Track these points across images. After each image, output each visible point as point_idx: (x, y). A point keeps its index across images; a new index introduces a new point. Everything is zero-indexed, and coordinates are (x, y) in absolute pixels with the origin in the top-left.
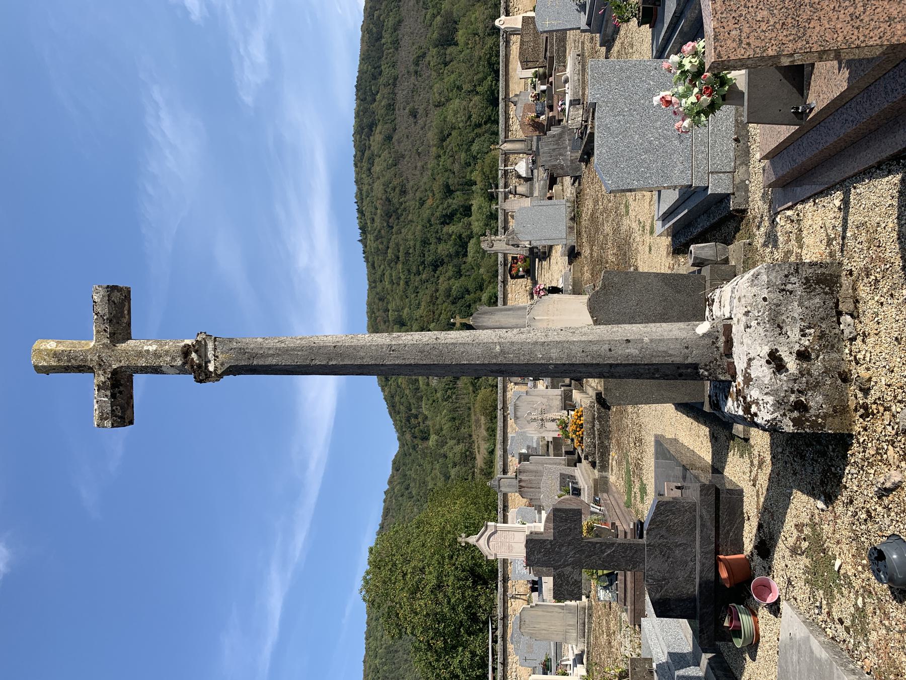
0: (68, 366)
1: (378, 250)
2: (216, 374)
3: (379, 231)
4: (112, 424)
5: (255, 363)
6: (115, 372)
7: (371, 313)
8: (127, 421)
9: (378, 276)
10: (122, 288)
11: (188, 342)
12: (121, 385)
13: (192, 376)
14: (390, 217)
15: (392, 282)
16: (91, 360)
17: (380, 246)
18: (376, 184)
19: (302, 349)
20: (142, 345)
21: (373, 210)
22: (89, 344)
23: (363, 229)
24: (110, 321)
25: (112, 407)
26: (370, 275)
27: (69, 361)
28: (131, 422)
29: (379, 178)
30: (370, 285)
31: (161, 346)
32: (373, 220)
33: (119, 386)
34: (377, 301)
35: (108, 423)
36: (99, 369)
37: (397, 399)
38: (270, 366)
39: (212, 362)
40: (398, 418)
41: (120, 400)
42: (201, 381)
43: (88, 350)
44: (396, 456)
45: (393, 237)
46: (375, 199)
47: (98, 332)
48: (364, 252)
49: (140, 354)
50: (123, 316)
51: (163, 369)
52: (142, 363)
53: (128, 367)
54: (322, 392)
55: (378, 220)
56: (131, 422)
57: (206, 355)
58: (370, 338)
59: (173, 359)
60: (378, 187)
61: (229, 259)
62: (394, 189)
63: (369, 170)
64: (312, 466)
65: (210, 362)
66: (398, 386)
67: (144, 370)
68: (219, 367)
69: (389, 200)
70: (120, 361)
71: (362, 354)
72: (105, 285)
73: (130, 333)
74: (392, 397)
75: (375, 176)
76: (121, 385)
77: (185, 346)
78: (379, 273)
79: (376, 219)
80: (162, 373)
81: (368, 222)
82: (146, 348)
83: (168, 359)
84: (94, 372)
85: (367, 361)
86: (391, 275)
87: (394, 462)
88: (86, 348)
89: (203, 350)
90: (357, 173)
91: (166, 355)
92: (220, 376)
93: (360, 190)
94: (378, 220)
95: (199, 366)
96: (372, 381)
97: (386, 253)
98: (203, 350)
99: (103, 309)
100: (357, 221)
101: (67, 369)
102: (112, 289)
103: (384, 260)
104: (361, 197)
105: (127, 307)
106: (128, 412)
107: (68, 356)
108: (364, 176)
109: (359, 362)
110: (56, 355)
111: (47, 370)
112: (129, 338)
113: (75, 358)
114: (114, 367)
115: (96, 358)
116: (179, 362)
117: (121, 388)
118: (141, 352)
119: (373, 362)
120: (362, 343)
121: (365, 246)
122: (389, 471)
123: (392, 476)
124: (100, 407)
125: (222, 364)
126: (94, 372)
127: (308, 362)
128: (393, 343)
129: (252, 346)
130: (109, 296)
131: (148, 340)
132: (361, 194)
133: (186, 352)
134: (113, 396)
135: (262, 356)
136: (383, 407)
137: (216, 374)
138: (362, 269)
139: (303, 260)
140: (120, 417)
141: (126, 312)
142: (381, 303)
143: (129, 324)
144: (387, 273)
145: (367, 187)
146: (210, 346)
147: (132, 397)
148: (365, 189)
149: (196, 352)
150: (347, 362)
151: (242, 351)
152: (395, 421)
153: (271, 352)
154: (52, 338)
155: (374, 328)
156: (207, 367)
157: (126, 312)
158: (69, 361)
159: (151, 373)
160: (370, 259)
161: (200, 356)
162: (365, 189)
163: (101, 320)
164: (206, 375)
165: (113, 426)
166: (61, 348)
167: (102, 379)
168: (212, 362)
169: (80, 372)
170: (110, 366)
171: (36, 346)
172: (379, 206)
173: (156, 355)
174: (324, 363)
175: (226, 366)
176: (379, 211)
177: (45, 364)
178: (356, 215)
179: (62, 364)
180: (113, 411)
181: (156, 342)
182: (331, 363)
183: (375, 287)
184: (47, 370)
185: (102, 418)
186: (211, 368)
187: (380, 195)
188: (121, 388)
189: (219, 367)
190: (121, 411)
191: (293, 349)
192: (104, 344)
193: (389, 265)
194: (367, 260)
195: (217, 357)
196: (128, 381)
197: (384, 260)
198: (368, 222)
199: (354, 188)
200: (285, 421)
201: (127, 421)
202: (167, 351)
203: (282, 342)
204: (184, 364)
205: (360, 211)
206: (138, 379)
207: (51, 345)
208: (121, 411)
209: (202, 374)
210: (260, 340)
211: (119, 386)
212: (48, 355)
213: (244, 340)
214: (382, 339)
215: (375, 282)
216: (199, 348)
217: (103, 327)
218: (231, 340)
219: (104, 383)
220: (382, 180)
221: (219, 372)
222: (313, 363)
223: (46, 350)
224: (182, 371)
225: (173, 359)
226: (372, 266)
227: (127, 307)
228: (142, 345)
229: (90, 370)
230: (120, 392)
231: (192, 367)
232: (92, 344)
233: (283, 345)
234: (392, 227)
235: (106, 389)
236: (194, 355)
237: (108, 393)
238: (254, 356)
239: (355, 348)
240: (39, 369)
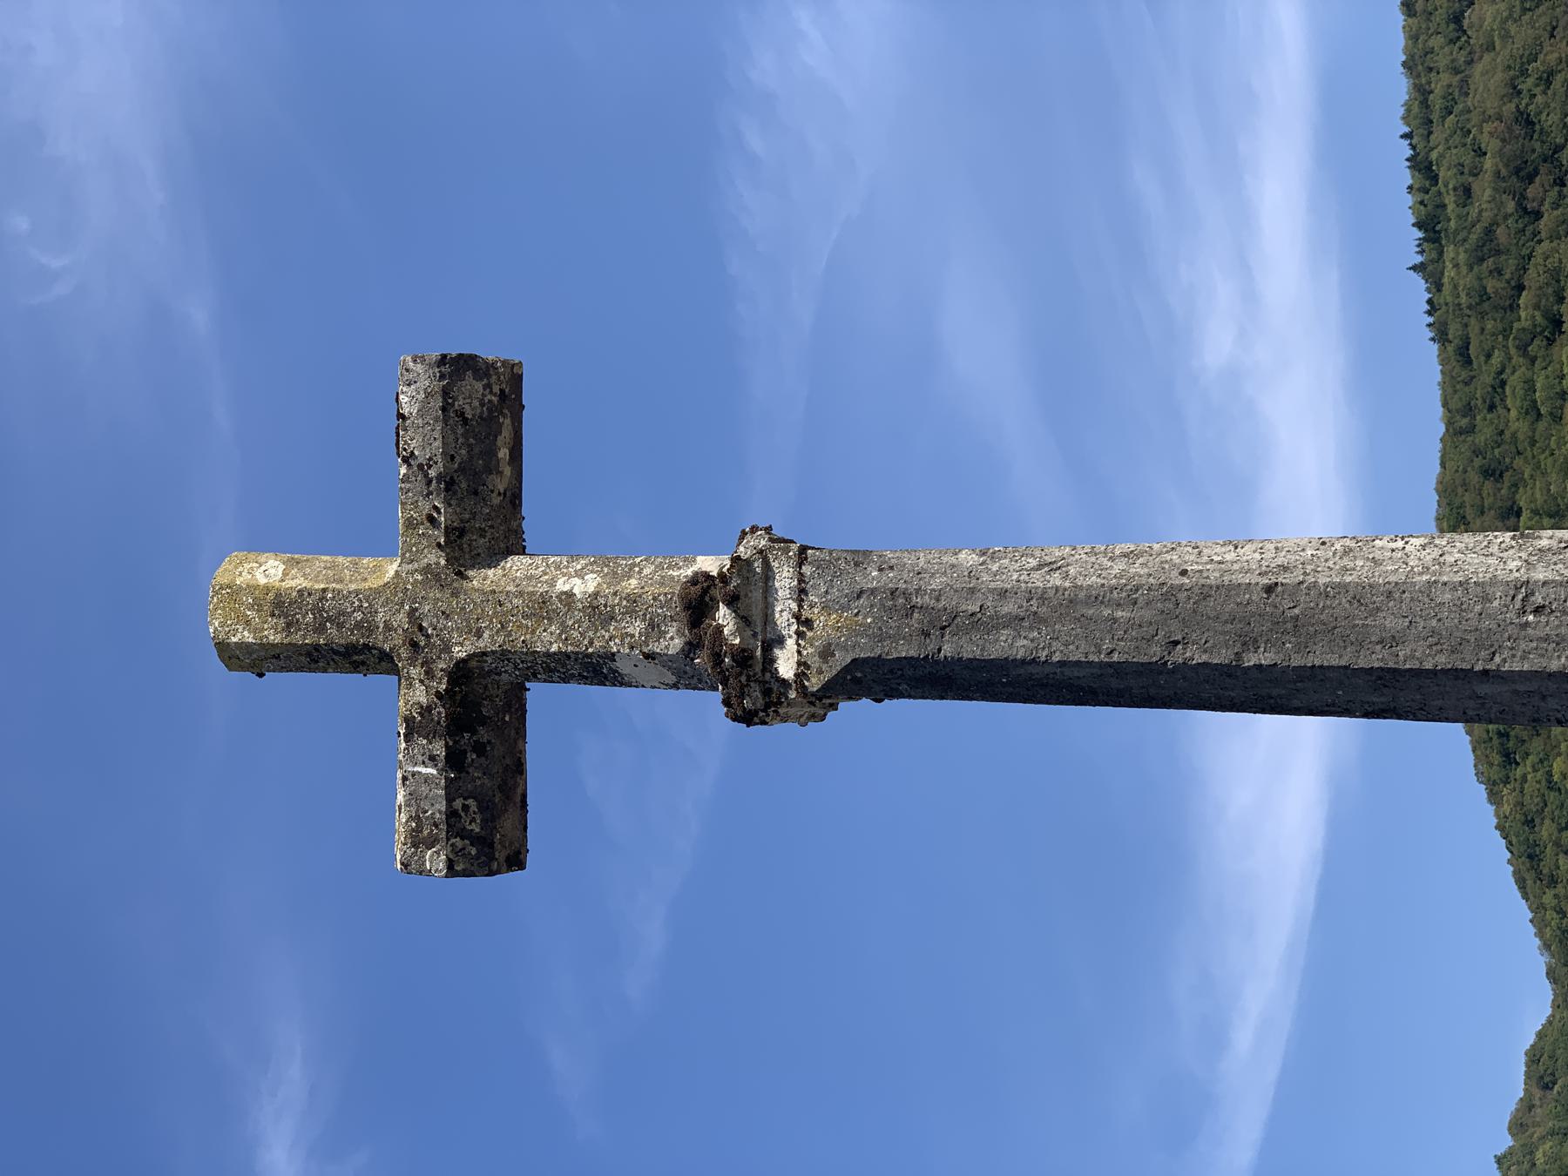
0: (317, 647)
1: (1484, 296)
2: (802, 690)
3: (1489, 231)
4: (450, 865)
5: (948, 650)
6: (461, 673)
7: (1447, 490)
8: (501, 855)
9: (1480, 390)
10: (491, 366)
11: (710, 564)
12: (483, 721)
13: (718, 696)
14: (1530, 178)
15: (1532, 411)
16: (388, 627)
17: (1491, 285)
18: (1478, 68)
19: (1130, 594)
20: (552, 579)
21: (1468, 159)
22: (377, 573)
23: (1430, 227)
24: (449, 484)
25: (450, 799)
26: (1450, 386)
27: (320, 629)
28: (516, 861)
29: (1490, 47)
30: (1449, 423)
31: (615, 577)
32: (1467, 191)
33: (479, 723)
34: (1474, 478)
35: (435, 860)
36: (412, 661)
37: (1546, 830)
38: (1003, 665)
39: (791, 643)
40: (1548, 899)
41: (478, 778)
42: (748, 718)
43: (377, 592)
44: (1541, 1035)
45: (1540, 250)
46: (1475, 118)
47: (410, 524)
48: (1433, 307)
49: (543, 607)
50: (492, 468)
51: (623, 666)
52: (549, 640)
53: (504, 655)
54: (1275, 778)
55: (1484, 191)
56: (516, 861)
57: (768, 618)
58: (1430, 555)
59: (654, 628)
60: (1487, 80)
61: (981, 346)
62: (1547, 79)
63: (1457, 19)
64: (1243, 1038)
65: (780, 641)
66: (1551, 785)
67: (561, 668)
68: (815, 662)
69: (1527, 121)
70: (479, 634)
71: (1392, 623)
72: (435, 355)
73: (519, 533)
74: (1530, 823)
75: (1477, 39)
76: (483, 721)
77: (694, 580)
78: (1487, 378)
79: (1475, 187)
80: (617, 679)
81: (1450, 200)
82: (562, 585)
83: (637, 627)
84: (395, 671)
85: (1414, 655)
86: (1530, 386)
87: (1534, 1057)
88: (374, 583)
89: (757, 595)
90: (1413, 37)
91: (631, 612)
92: (822, 701)
93: (1422, 93)
94: (1484, 191)
95: (743, 658)
96: (1447, 747)
97: (1514, 307)
98: (757, 595)
99: (426, 442)
100: (1409, 200)
101: (315, 658)
102: (456, 367)
103: (1506, 332)
104: (1423, 117)
105: (506, 433)
106: (508, 823)
107: (317, 610)
108: (1436, 42)
109: (1375, 658)
110: (281, 605)
111: (252, 660)
112: (516, 546)
113: (338, 619)
114: (459, 652)
115: (401, 620)
116: (673, 641)
117: (483, 734)
118: (544, 600)
119: (1442, 661)
120: (1392, 572)
121: (1436, 284)
122: (1515, 1085)
123: (1527, 1105)
124: (412, 797)
125: (826, 653)
126: (395, 671)
127: (1154, 653)
128: (1540, 575)
129: (937, 583)
130: (445, 393)
131: (574, 557)
132: (1425, 104)
133: (698, 601)
134: (454, 760)
135: (977, 622)
136: (1492, 859)
137: (802, 690)
138: (1423, 366)
139: (1217, 344)
140: (475, 840)
141: (503, 453)
142: (1489, 486)
143: (514, 498)
144: (1514, 381)
145: (1445, 78)
146: (784, 580)
147: (519, 768)
148: (1438, 89)
149: (732, 601)
150: (1323, 656)
151: (899, 602)
152: (1538, 909)
153: (1009, 608)
154: (275, 549)
155: (1457, 516)
156: (769, 661)
157: (503, 453)
158: (320, 629)
159: (582, 679)
160: (1454, 330)
161: (744, 620)
162: (1438, 89)
163: (420, 485)
164: (767, 692)
165: (451, 871)
166: (298, 582)
167: (420, 695)
168: (791, 643)
169: (356, 667)
170: (447, 648)
171: (222, 576)
172: (1492, 145)
173: (598, 613)
174: (1222, 657)
175: (841, 659)
176: (1488, 163)
177: (249, 638)
178: (1406, 177)
179: (297, 638)
180: (451, 814)
181: (602, 561)
182: (1251, 660)
183: (1471, 430)
184: (252, 660)
185: (418, 840)
186: (786, 666)
187: (1491, 106)
188: (483, 734)
189: (815, 662)
190: (484, 821)
191: (1097, 598)
192: (426, 570)
193: (1523, 349)
194: (1441, 334)
195: (808, 623)
196: (508, 707)
197: (1506, 332)
198: (1450, 200)
199: (1400, 88)
200: (1144, 875)
201: (501, 855)
202: (633, 599)
203: (1052, 567)
204: (691, 648)
205: (1422, 166)
206: (538, 695)
207: (269, 571)
208: (484, 821)
209: (753, 693)
210: (968, 558)
211: (479, 723)
212: (257, 605)
213: (908, 560)
214: (1493, 557)
215: (1468, 410)
216: (744, 586)
217: (425, 506)
218: (859, 558)
219: (426, 710)
220: (1503, 55)
221: (814, 683)
222: (1178, 656)
223: (252, 588)
224: (683, 675)
225: (654, 628)
226: (1459, 355)
227: (506, 433)
228: (552, 579)
229: (384, 662)
230: (480, 749)
231: (717, 659)
232: (392, 568)
233: (1056, 580)
234: (1538, 215)
235: (430, 736)
236: (724, 616)
237: (439, 748)
238: (945, 622)
239: (1359, 595)
240: (232, 656)
